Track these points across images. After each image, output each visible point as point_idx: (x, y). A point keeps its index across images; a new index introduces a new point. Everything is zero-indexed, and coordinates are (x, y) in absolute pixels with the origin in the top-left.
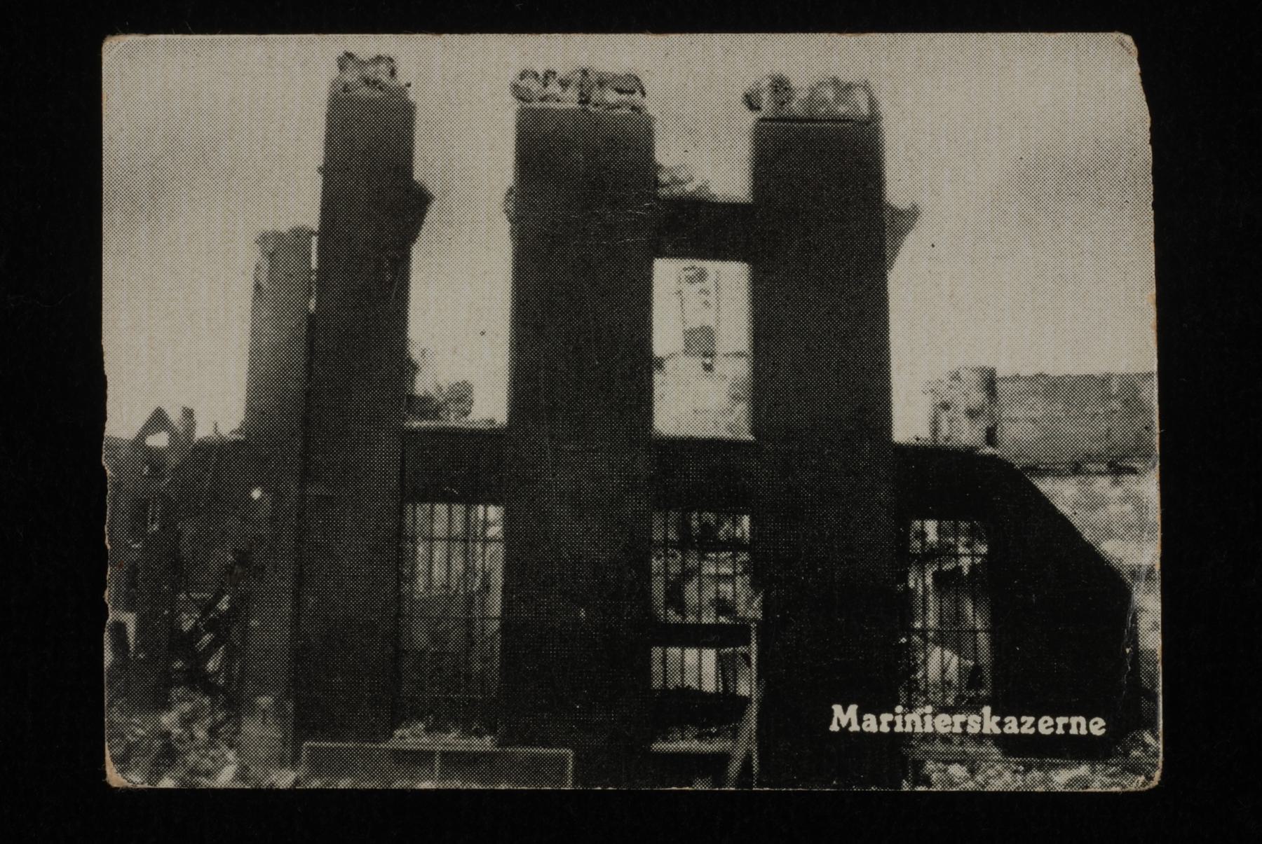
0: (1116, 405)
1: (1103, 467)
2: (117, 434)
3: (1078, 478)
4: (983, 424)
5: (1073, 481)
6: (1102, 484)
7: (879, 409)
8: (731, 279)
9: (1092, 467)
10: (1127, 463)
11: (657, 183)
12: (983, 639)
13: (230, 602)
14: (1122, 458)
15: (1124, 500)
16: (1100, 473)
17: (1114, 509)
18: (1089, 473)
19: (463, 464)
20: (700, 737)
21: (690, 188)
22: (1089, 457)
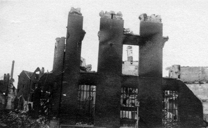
0: (200, 72)
1: (198, 82)
5: (193, 85)
9: (196, 82)
10: (202, 82)
14: (201, 81)
15: (201, 88)
16: (197, 84)
18: (196, 83)
21: (129, 33)
22: (195, 81)
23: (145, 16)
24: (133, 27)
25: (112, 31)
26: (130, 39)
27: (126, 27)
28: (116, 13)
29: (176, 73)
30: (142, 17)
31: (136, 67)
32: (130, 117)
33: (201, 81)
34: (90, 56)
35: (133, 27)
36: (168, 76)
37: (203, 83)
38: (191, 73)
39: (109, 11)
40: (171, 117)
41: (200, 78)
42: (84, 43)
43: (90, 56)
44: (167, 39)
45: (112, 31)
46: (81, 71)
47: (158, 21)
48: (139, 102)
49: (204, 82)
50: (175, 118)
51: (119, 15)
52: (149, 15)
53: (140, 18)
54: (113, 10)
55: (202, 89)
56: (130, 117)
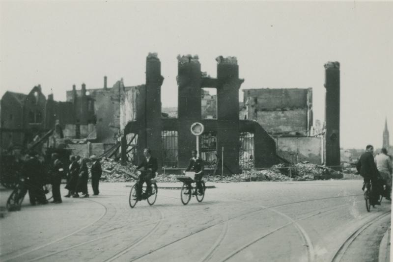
0: (283, 95)
1: (280, 109)
2: (169, 106)
3: (275, 112)
4: (254, 108)
5: (274, 112)
6: (280, 113)
7: (80, 194)
8: (81, 127)
9: (278, 109)
10: (285, 109)
11: (202, 75)
12: (253, 151)
13: (82, 174)
14: (284, 107)
15: (284, 117)
16: (279, 111)
17: (282, 119)
18: (277, 111)
19: (169, 124)
20: (209, 167)
21: (207, 76)
22: (277, 107)
23: (221, 57)
24: (210, 70)
25: (189, 71)
26: (209, 82)
27: (203, 70)
28: (193, 56)
29: (253, 106)
30: (219, 59)
31: (208, 101)
32: (205, 159)
33: (284, 107)
34: (170, 99)
35: (210, 70)
36: (244, 119)
37: (286, 110)
38: (271, 97)
39: (186, 55)
40: (247, 156)
41: (284, 103)
42: (164, 88)
43: (170, 99)
44: (242, 81)
45: (189, 71)
46: (163, 118)
47: (234, 62)
48: (205, 89)
49: (288, 109)
50: (251, 157)
51: (196, 58)
52: (225, 57)
53: (217, 60)
54: (189, 54)
55: (285, 119)
56: (205, 159)
